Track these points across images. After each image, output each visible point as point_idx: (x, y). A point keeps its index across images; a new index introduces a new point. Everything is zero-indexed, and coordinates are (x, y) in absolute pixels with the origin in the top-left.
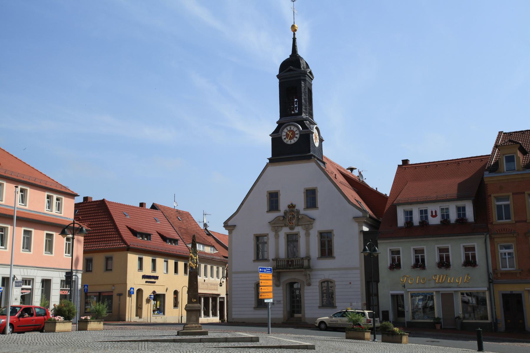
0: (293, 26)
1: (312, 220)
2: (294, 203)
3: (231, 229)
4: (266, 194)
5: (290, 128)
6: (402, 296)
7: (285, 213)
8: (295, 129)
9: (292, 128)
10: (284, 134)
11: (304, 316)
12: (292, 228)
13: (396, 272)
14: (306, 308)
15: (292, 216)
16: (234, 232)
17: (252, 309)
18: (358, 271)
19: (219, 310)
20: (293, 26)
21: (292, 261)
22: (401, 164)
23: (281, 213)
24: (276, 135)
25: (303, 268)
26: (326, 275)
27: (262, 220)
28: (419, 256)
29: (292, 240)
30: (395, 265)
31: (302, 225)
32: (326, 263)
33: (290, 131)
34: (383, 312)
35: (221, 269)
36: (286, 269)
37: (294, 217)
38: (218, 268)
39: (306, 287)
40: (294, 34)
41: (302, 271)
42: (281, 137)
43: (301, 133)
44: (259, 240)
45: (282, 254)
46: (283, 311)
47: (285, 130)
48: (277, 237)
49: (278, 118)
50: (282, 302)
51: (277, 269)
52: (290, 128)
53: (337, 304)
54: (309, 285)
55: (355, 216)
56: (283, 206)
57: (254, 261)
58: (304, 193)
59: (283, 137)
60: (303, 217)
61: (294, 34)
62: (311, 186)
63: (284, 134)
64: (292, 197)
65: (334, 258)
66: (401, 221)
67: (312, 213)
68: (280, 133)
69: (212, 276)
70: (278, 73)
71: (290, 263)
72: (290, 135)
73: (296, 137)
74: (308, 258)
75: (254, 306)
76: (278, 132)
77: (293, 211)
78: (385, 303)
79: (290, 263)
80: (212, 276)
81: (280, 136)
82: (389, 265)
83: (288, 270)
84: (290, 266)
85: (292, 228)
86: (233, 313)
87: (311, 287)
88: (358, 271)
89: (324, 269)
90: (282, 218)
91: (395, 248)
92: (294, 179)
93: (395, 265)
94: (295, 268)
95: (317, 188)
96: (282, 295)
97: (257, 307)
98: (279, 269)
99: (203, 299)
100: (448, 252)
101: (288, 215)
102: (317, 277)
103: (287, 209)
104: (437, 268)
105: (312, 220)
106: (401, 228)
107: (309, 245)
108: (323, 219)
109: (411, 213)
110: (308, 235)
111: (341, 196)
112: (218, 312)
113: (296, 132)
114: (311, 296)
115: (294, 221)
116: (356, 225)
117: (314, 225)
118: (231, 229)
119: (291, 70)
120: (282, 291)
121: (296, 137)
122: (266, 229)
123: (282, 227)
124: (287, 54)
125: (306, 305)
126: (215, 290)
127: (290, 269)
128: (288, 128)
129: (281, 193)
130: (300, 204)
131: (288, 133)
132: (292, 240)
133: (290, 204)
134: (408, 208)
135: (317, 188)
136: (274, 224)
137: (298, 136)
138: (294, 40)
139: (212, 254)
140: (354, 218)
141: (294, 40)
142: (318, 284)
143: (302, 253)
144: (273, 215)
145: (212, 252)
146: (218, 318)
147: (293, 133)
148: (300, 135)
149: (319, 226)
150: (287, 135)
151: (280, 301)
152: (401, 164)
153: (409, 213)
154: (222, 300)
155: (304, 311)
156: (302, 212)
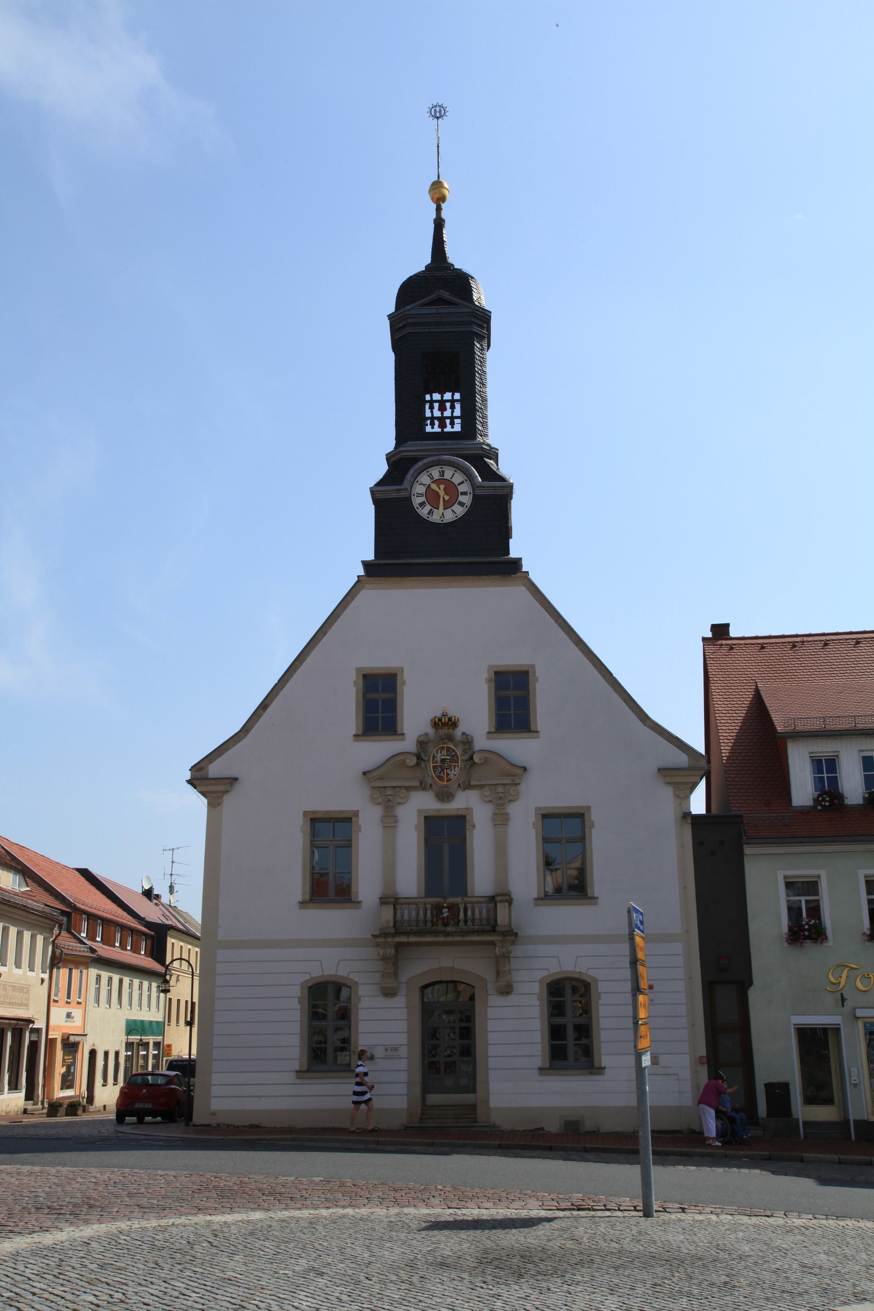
0: (437, 185)
1: (516, 773)
2: (453, 712)
3: (221, 788)
4: (353, 676)
5: (442, 473)
6: (837, 1030)
7: (422, 744)
8: (458, 478)
9: (449, 473)
10: (419, 489)
11: (487, 1100)
12: (445, 796)
13: (812, 952)
14: (492, 1075)
15: (445, 754)
16: (228, 801)
17: (291, 1077)
18: (678, 948)
19: (26, 1070)
20: (437, 185)
21: (453, 908)
22: (709, 635)
23: (408, 744)
24: (391, 490)
25: (493, 931)
26: (566, 961)
27: (338, 766)
28: (800, 901)
29: (445, 840)
30: (806, 928)
31: (481, 787)
32: (566, 917)
33: (438, 482)
34: (769, 1086)
35: (40, 939)
36: (435, 933)
37: (454, 758)
38: (33, 937)
39: (494, 1000)
40: (439, 209)
41: (492, 943)
42: (409, 499)
43: (479, 492)
44: (330, 833)
45: (409, 880)
46: (409, 1084)
47: (424, 479)
48: (390, 822)
49: (390, 444)
50: (403, 1052)
51: (397, 932)
52: (442, 473)
53: (605, 1061)
54: (507, 990)
55: (663, 764)
56: (415, 718)
57: (303, 904)
58: (489, 680)
59: (417, 501)
60: (486, 761)
61: (439, 209)
62: (512, 660)
63: (421, 489)
64: (446, 688)
65: (594, 899)
66: (803, 788)
67: (514, 747)
68: (406, 484)
69: (18, 965)
70: (392, 309)
71: (445, 913)
72: (442, 493)
73: (462, 504)
74: (501, 897)
75: (296, 1066)
76: (400, 481)
77: (450, 738)
78: (776, 1057)
79: (445, 913)
80: (18, 965)
81: (404, 494)
82: (785, 929)
83: (441, 939)
84: (446, 924)
85: (445, 796)
86: (214, 1091)
87: (512, 999)
88: (678, 948)
89: (559, 940)
90: (414, 761)
91: (802, 871)
92: (446, 645)
93: (806, 928)
94: (464, 933)
95: (533, 666)
96: (403, 1026)
97: (308, 1071)
98: (407, 933)
99: (9, 1035)
100: (816, 892)
101: (432, 750)
102: (536, 968)
103: (431, 731)
104: (786, 944)
105: (516, 773)
106: (804, 812)
107: (505, 857)
108: (552, 768)
109: (831, 764)
110: (501, 819)
111: (616, 698)
112: (24, 1074)
113: (461, 489)
114: (512, 1029)
115: (454, 773)
116: (668, 793)
117: (522, 788)
118: (221, 788)
119: (440, 301)
120: (403, 1014)
121: (462, 504)
122: (346, 796)
123: (409, 789)
124: (419, 260)
125: (492, 1063)
126: (21, 1005)
127: (446, 934)
128: (435, 472)
129: (406, 676)
130: (476, 718)
131: (434, 487)
132: (445, 840)
133: (439, 715)
134: (825, 748)
135: (533, 666)
136: (381, 778)
137: (467, 500)
138: (439, 224)
139: (16, 894)
140: (660, 770)
141: (439, 224)
142: (536, 988)
143: (481, 879)
144: (379, 750)
145: (17, 889)
146: (22, 1094)
147: (451, 489)
148: (475, 498)
149: (540, 793)
150: (432, 497)
151: (395, 1049)
152: (709, 635)
153: (825, 767)
154: (34, 1038)
155: (487, 1083)
156: (481, 742)
